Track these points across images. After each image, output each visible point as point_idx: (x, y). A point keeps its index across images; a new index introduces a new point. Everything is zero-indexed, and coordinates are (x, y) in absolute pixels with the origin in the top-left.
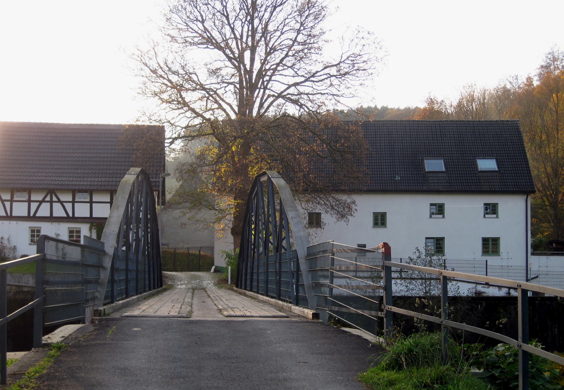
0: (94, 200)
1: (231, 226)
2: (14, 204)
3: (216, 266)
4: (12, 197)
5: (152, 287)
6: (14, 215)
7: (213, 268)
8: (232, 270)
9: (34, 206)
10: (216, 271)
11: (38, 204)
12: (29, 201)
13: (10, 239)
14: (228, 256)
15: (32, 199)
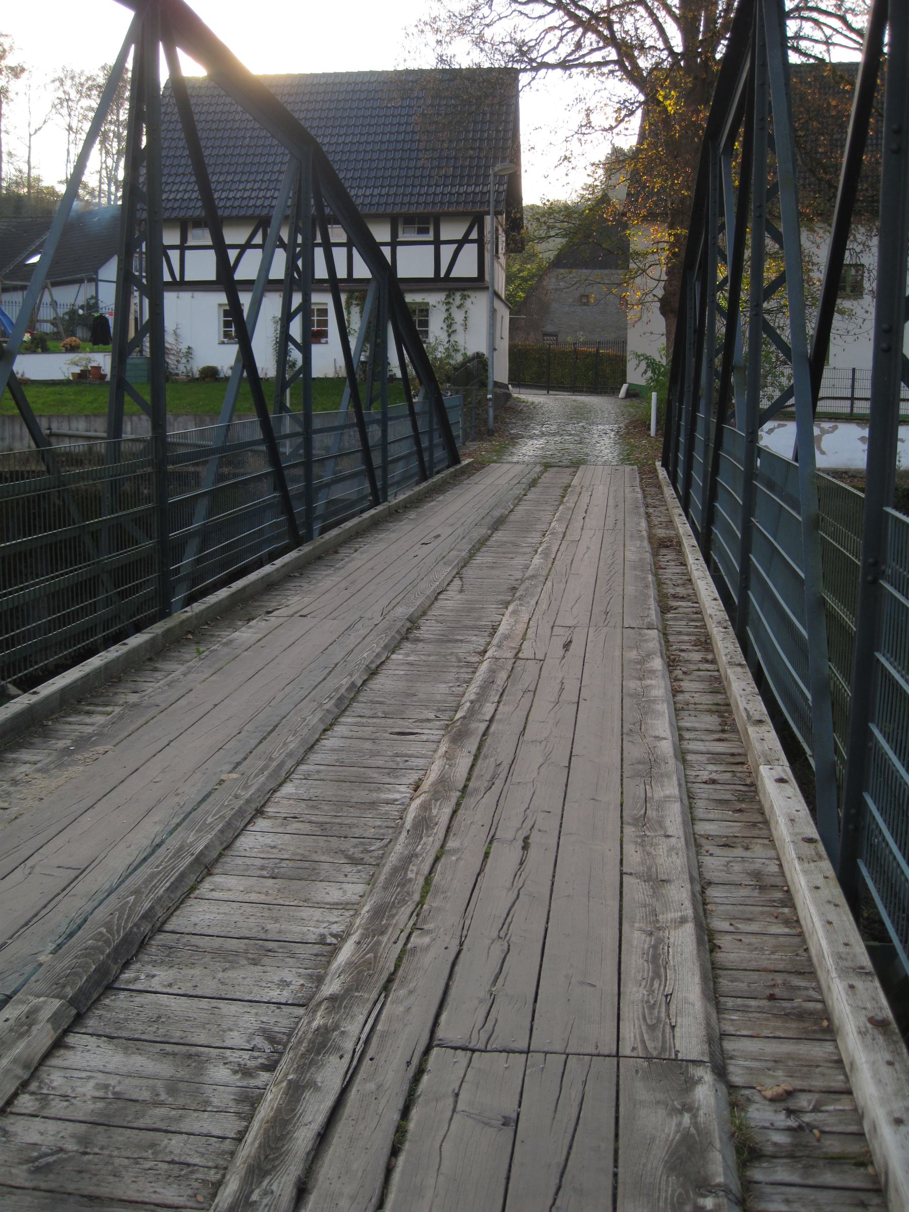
0: (442, 238)
1: (660, 293)
2: (188, 253)
3: (630, 384)
4: (184, 238)
5: (22, 667)
6: (187, 278)
7: (625, 387)
8: (659, 401)
9: (447, 252)
10: (629, 395)
11: (455, 246)
12: (437, 243)
13: (178, 331)
14: (652, 365)
15: (443, 237)
